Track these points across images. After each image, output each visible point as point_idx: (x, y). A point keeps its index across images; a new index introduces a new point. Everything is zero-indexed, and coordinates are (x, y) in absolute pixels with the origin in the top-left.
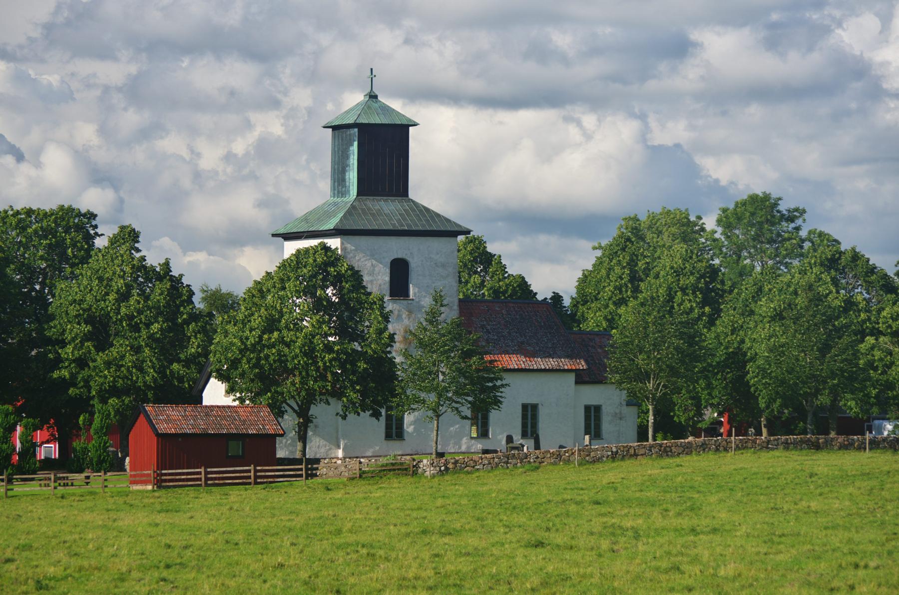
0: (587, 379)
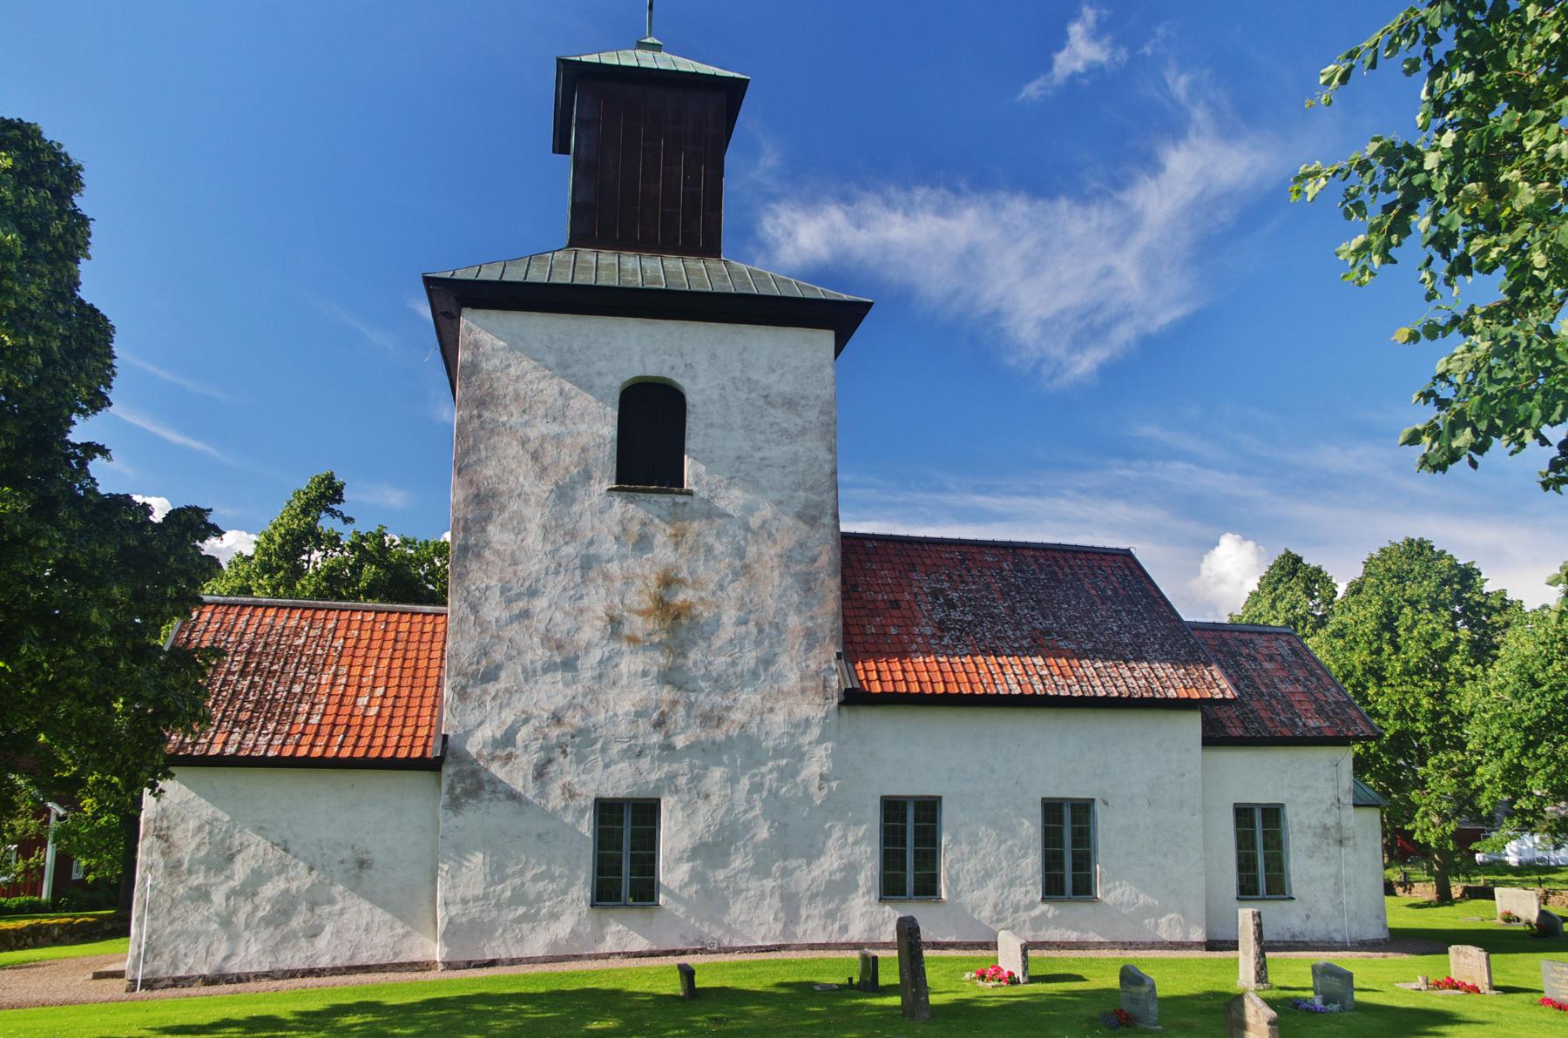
0: (1239, 732)
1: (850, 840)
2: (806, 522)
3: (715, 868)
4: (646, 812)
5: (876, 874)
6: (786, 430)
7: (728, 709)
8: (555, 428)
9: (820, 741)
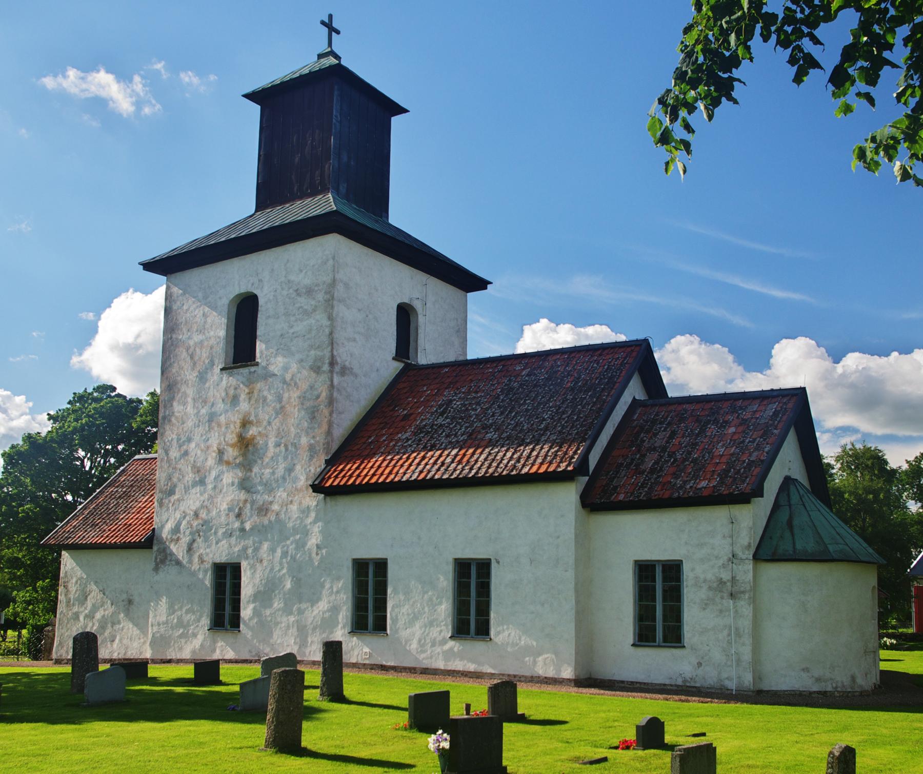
1: (335, 590)
2: (315, 371)
3: (265, 608)
4: (236, 569)
5: (349, 614)
6: (306, 310)
7: (271, 503)
8: (201, 337)
9: (315, 522)
